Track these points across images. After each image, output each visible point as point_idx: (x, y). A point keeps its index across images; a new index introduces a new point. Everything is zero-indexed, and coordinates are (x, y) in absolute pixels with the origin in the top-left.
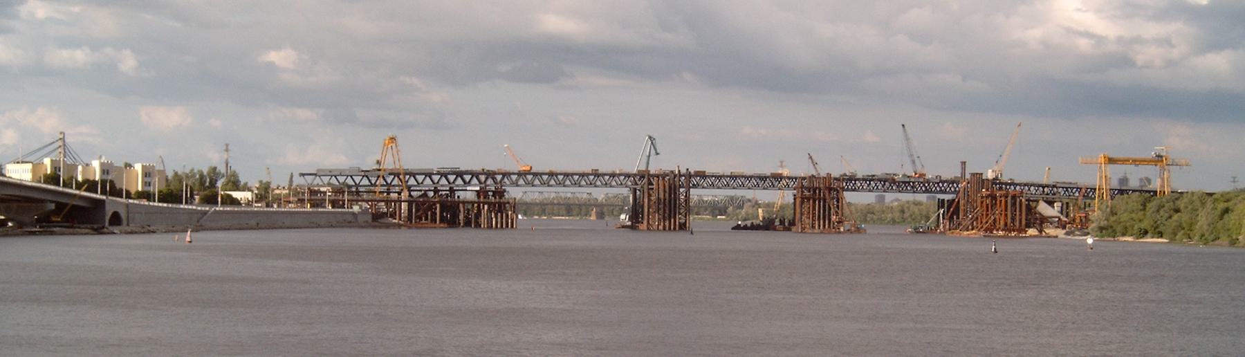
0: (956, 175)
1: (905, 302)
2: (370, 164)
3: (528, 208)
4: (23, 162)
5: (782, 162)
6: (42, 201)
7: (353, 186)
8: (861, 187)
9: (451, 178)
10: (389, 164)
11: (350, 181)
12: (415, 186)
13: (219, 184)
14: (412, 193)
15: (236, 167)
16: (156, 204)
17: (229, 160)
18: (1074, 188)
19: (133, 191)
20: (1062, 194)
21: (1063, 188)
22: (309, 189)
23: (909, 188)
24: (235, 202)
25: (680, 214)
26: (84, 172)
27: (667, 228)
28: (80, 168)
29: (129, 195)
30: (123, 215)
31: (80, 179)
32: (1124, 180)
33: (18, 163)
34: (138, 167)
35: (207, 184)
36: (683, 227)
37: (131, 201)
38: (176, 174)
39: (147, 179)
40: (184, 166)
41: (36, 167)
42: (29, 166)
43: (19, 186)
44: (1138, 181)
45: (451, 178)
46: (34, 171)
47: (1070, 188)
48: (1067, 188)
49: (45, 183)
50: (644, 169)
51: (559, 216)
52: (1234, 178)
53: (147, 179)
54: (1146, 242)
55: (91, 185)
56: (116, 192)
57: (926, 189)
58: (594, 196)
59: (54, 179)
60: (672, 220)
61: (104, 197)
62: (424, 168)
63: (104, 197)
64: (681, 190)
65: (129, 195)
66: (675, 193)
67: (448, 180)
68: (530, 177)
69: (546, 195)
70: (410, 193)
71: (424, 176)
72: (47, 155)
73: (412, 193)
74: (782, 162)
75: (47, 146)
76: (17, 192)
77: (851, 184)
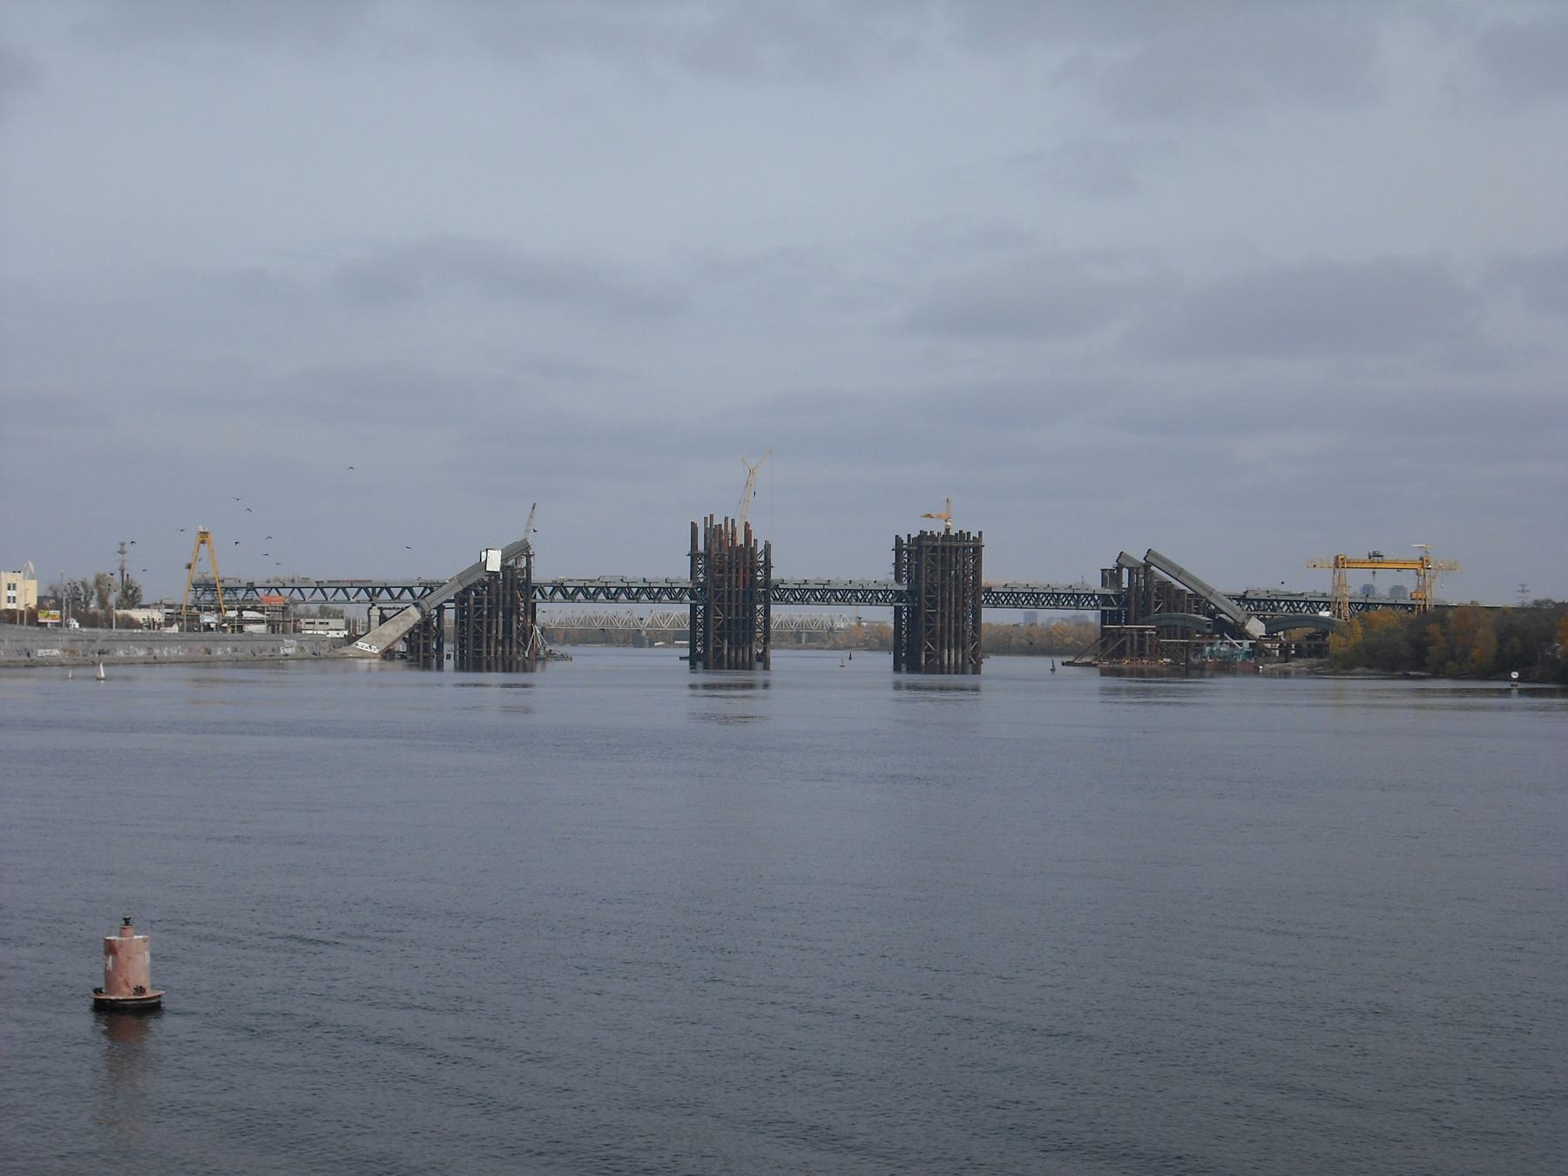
3: (805, 638)
8: (1026, 602)
9: (330, 592)
14: (385, 612)
15: (137, 579)
17: (125, 566)
18: (1301, 601)
20: (1284, 610)
21: (1286, 601)
23: (1092, 603)
27: (953, 670)
32: (1367, 590)
40: (62, 575)
47: (1316, 602)
50: (987, 578)
51: (1541, 689)
52: (1523, 586)
60: (953, 661)
62: (1171, 560)
64: (759, 607)
66: (751, 611)
67: (346, 594)
70: (381, 612)
71: (335, 589)
73: (385, 612)
77: (993, 598)
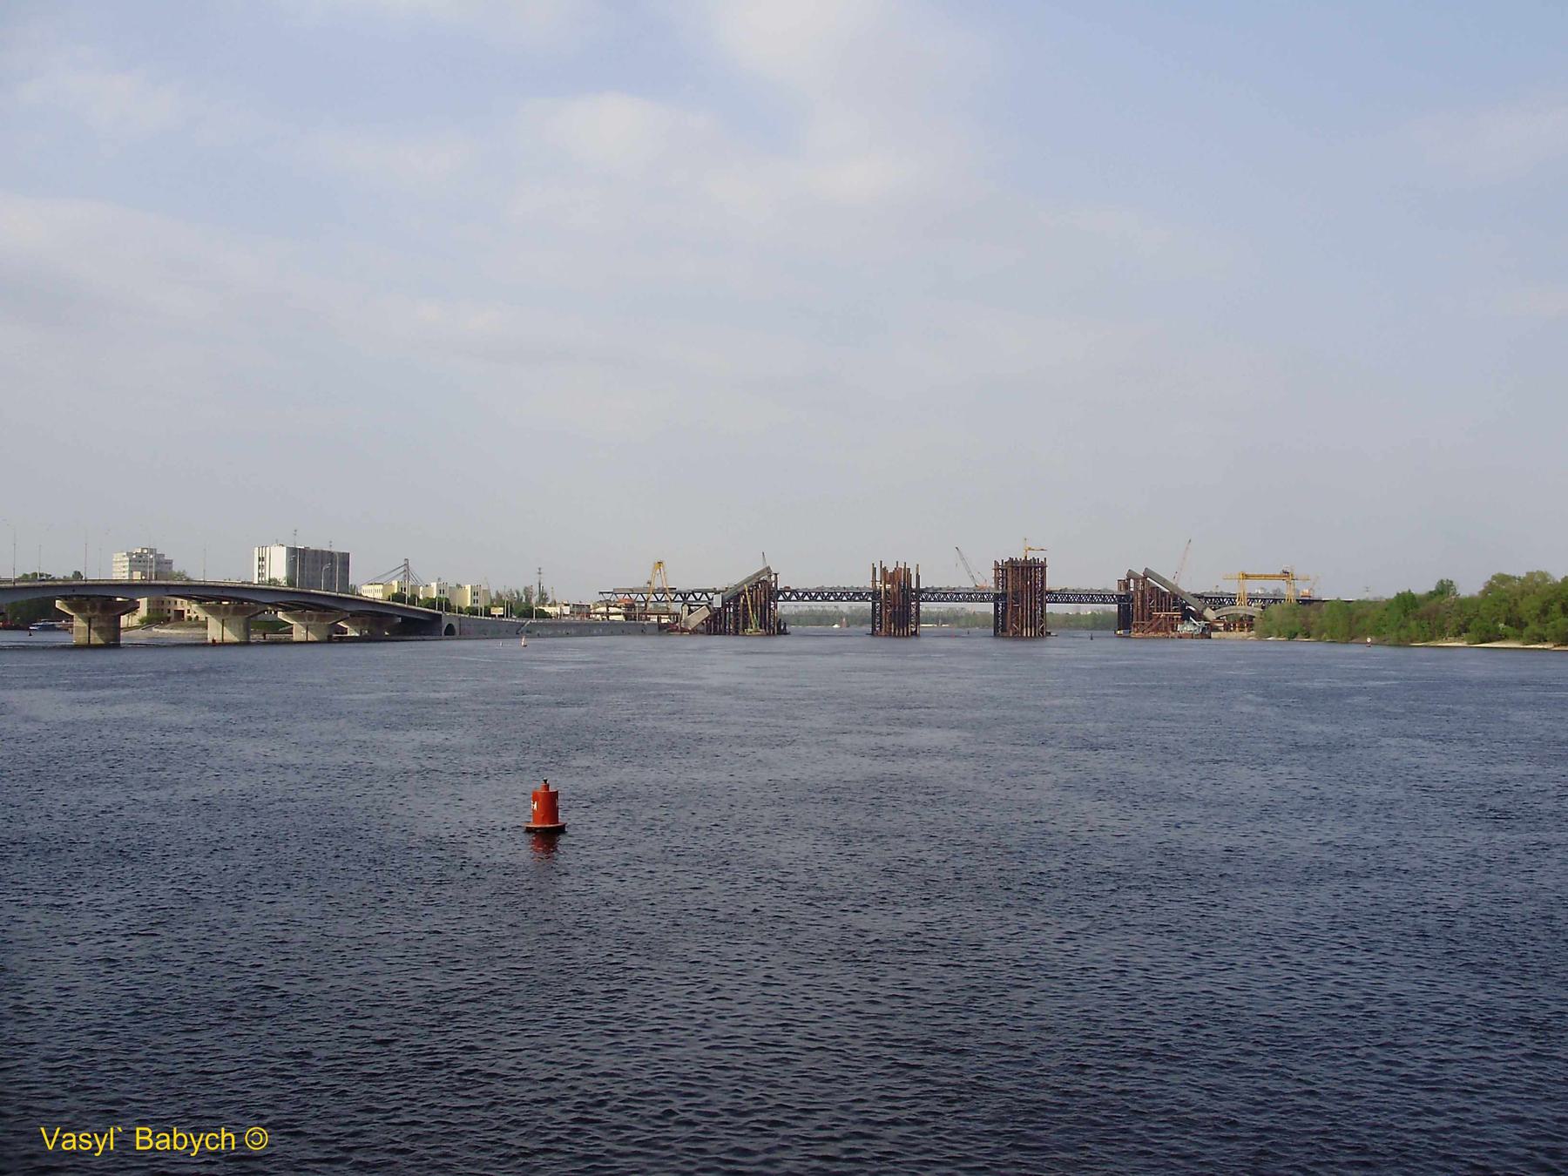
0: (67, 576)
1: (1194, 967)
2: (642, 584)
4: (375, 584)
5: (540, 569)
6: (392, 615)
7: (642, 602)
10: (657, 584)
11: (640, 598)
12: (693, 602)
13: (534, 601)
15: (547, 588)
16: (483, 618)
19: (464, 608)
22: (459, 608)
24: (545, 615)
25: (912, 623)
26: (423, 593)
28: (421, 588)
29: (460, 612)
30: (456, 627)
31: (421, 597)
33: (372, 584)
34: (468, 587)
35: (524, 600)
36: (915, 634)
37: (462, 615)
38: (498, 594)
39: (475, 597)
41: (387, 585)
42: (381, 587)
43: (373, 603)
44: (73, 573)
45: (698, 595)
46: (383, 591)
48: (1231, 598)
49: (393, 601)
53: (475, 597)
54: (741, 1172)
55: (431, 603)
56: (449, 608)
57: (1112, 596)
58: (840, 608)
59: (399, 597)
61: (441, 612)
63: (441, 612)
65: (460, 612)
67: (695, 597)
68: (788, 594)
69: (800, 608)
72: (393, 578)
74: (540, 569)
75: (390, 573)
76: (370, 609)
